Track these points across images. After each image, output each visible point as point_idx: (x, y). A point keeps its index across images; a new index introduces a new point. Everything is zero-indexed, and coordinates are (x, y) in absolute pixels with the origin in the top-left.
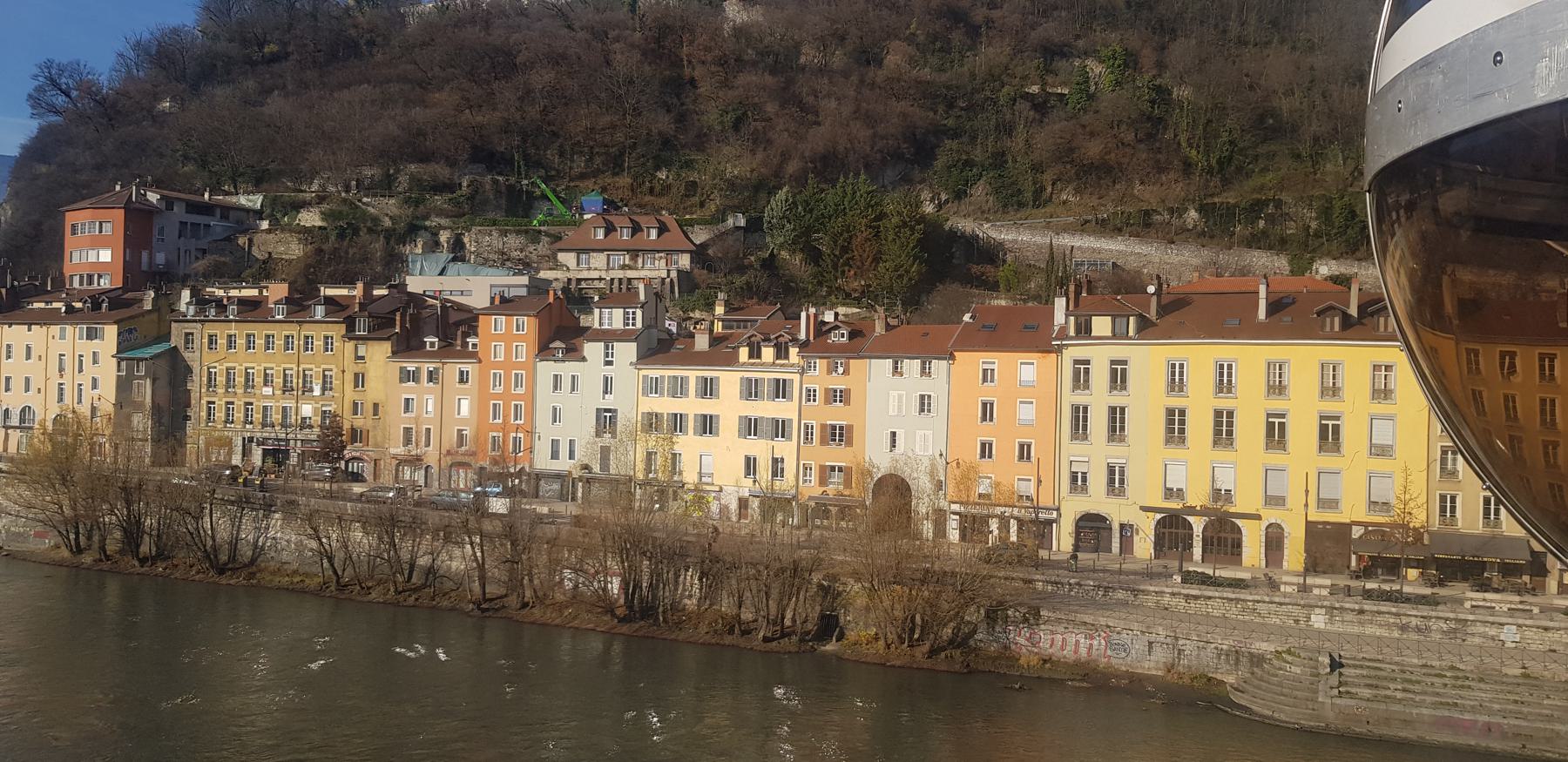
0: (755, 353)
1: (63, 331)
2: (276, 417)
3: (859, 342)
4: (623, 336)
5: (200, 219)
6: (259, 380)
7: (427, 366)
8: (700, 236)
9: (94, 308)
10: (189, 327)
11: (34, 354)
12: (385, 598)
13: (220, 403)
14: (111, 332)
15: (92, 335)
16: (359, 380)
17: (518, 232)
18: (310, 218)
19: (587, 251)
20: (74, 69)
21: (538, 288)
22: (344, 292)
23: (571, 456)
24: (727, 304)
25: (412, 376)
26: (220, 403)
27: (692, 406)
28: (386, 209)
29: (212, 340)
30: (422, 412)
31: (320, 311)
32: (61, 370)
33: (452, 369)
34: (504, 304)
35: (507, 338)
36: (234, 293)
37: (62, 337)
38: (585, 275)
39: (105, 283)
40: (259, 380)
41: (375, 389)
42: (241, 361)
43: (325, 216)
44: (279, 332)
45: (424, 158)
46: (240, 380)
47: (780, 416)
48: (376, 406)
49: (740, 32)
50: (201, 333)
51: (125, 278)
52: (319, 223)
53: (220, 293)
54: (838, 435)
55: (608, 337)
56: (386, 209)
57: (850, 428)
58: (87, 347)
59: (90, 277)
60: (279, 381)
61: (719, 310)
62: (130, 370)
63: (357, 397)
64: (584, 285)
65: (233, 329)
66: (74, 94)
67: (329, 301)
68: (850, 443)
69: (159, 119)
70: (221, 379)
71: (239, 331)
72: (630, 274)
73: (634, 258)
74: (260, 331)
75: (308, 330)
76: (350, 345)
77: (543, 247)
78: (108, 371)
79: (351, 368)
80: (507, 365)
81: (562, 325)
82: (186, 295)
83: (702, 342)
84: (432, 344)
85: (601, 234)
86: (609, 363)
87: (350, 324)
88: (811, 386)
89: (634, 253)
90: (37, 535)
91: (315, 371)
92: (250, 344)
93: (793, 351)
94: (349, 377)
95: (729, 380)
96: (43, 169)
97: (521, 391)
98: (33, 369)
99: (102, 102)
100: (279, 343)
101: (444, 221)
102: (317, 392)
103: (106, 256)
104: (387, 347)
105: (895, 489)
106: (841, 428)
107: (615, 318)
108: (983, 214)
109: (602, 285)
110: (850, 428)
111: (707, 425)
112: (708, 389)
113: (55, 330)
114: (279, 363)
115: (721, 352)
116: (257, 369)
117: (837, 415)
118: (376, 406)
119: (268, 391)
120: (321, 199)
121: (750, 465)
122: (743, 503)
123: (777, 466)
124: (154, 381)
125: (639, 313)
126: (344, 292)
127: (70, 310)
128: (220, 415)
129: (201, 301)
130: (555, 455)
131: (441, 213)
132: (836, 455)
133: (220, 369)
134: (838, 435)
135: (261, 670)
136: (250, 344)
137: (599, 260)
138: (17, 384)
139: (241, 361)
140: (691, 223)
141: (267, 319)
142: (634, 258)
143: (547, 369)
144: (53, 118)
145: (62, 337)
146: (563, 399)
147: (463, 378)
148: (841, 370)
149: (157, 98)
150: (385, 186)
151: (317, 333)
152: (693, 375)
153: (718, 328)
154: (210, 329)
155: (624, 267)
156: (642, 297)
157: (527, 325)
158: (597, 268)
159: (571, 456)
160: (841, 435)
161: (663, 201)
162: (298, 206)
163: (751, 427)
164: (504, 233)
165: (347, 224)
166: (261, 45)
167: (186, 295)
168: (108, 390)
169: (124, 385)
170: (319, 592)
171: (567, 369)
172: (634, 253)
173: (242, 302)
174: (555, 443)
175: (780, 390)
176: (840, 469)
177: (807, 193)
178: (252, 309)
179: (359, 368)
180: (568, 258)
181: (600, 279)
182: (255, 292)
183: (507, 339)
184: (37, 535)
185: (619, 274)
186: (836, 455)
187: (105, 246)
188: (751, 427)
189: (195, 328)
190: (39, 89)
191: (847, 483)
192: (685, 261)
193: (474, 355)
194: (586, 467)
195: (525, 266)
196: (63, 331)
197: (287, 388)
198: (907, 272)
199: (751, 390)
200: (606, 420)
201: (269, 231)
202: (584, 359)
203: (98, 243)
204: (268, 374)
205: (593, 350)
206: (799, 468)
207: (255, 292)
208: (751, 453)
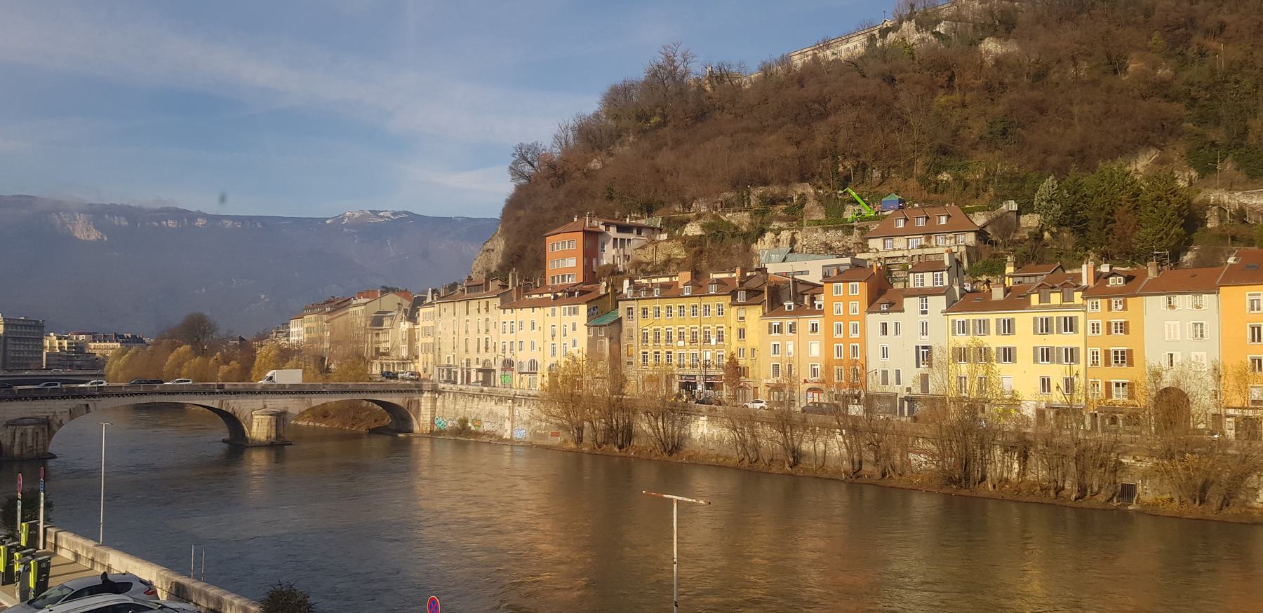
0: (1044, 299)
1: (553, 311)
2: (688, 361)
3: (1133, 287)
4: (935, 292)
5: (625, 236)
6: (675, 337)
7: (787, 322)
8: (980, 220)
9: (570, 295)
10: (630, 304)
11: (536, 327)
12: (771, 476)
13: (651, 353)
14: (583, 309)
15: (576, 312)
16: (742, 333)
17: (837, 229)
18: (693, 230)
19: (891, 236)
20: (533, 148)
21: (857, 265)
22: (726, 275)
23: (898, 382)
24: (1018, 266)
25: (779, 329)
26: (651, 353)
27: (994, 341)
28: (741, 219)
29: (645, 312)
30: (785, 354)
31: (713, 289)
32: (553, 336)
33: (805, 323)
34: (843, 276)
35: (846, 300)
36: (654, 281)
37: (553, 315)
38: (892, 254)
39: (572, 281)
40: (675, 337)
41: (752, 339)
42: (667, 324)
43: (703, 227)
44: (688, 303)
45: (766, 184)
46: (663, 337)
47: (1070, 345)
48: (753, 350)
49: (999, 62)
50: (637, 306)
51: (584, 277)
52: (699, 233)
53: (645, 281)
54: (1124, 358)
55: (924, 294)
56: (741, 219)
57: (1130, 352)
58: (569, 320)
59: (563, 276)
60: (688, 337)
61: (1010, 270)
62: (595, 334)
63: (740, 345)
64: (888, 262)
65: (658, 303)
66: (536, 164)
67: (719, 282)
68: (1131, 364)
69: (589, 174)
70: (651, 337)
71: (662, 304)
72: (927, 251)
73: (928, 239)
74: (675, 303)
75: (706, 301)
76: (734, 309)
77: (856, 236)
78: (582, 335)
79: (736, 325)
80: (846, 317)
81: (883, 290)
82: (626, 283)
83: (998, 294)
84: (790, 307)
85: (901, 224)
86: (924, 312)
87: (734, 294)
88: (1095, 321)
89: (928, 236)
90: (553, 435)
91: (713, 329)
92: (670, 313)
93: (1078, 296)
94: (734, 332)
95: (1024, 320)
96: (521, 213)
97: (858, 336)
98: (535, 336)
99: (552, 166)
100: (688, 311)
101: (784, 225)
102: (713, 342)
103: (572, 263)
104: (758, 310)
105: (1172, 402)
106: (1123, 352)
107: (929, 280)
108: (1231, 187)
109: (905, 261)
110: (1130, 352)
111: (1008, 355)
112: (1008, 327)
113: (548, 310)
114: (688, 324)
115: (1016, 300)
116: (674, 330)
117: (1119, 343)
118: (753, 350)
119: (681, 343)
120: (699, 216)
121: (1045, 384)
122: (1040, 413)
123: (1070, 385)
124: (611, 339)
125: (945, 274)
126: (726, 275)
127: (556, 297)
128: (651, 360)
129: (636, 288)
130: (885, 382)
131: (780, 219)
132: (1120, 374)
133: (650, 330)
134: (1124, 358)
135: (689, 529)
136: (670, 313)
137: (900, 242)
138: (527, 346)
139: (667, 324)
140: (972, 211)
141: (679, 296)
142: (928, 239)
143: (875, 320)
144: (523, 181)
145: (553, 315)
146: (890, 340)
147: (814, 328)
148: (1120, 307)
149: (588, 161)
150: (741, 204)
151: (713, 302)
152: (993, 317)
153: (1009, 282)
154: (643, 304)
155: (921, 247)
156: (947, 263)
157: (859, 290)
158: (901, 247)
159: (898, 382)
160: (1123, 358)
161: (946, 196)
162: (684, 223)
163: (1046, 355)
164: (826, 230)
165: (717, 232)
166: (648, 120)
167: (626, 283)
168: (583, 344)
169: (592, 343)
170: (736, 468)
171: (891, 319)
172: (928, 236)
173: (663, 286)
174: (885, 373)
175: (1070, 325)
176: (1124, 385)
177: (1069, 180)
178: (669, 291)
179: (741, 326)
180: (875, 243)
181: (903, 257)
182: (667, 280)
183: (847, 299)
184: (553, 435)
185: (920, 252)
186: (1120, 374)
187: (571, 256)
188: (1046, 355)
189: (633, 304)
190: (514, 163)
191: (1131, 396)
192: (971, 238)
193: (821, 312)
194: (909, 389)
195: (847, 252)
196: (553, 311)
197: (694, 341)
198: (1167, 235)
199: (1045, 327)
200: (924, 355)
201: (667, 241)
202: (903, 311)
203: (569, 254)
204: (682, 332)
205: (911, 304)
206: (1093, 381)
207: (667, 280)
208: (1046, 375)
